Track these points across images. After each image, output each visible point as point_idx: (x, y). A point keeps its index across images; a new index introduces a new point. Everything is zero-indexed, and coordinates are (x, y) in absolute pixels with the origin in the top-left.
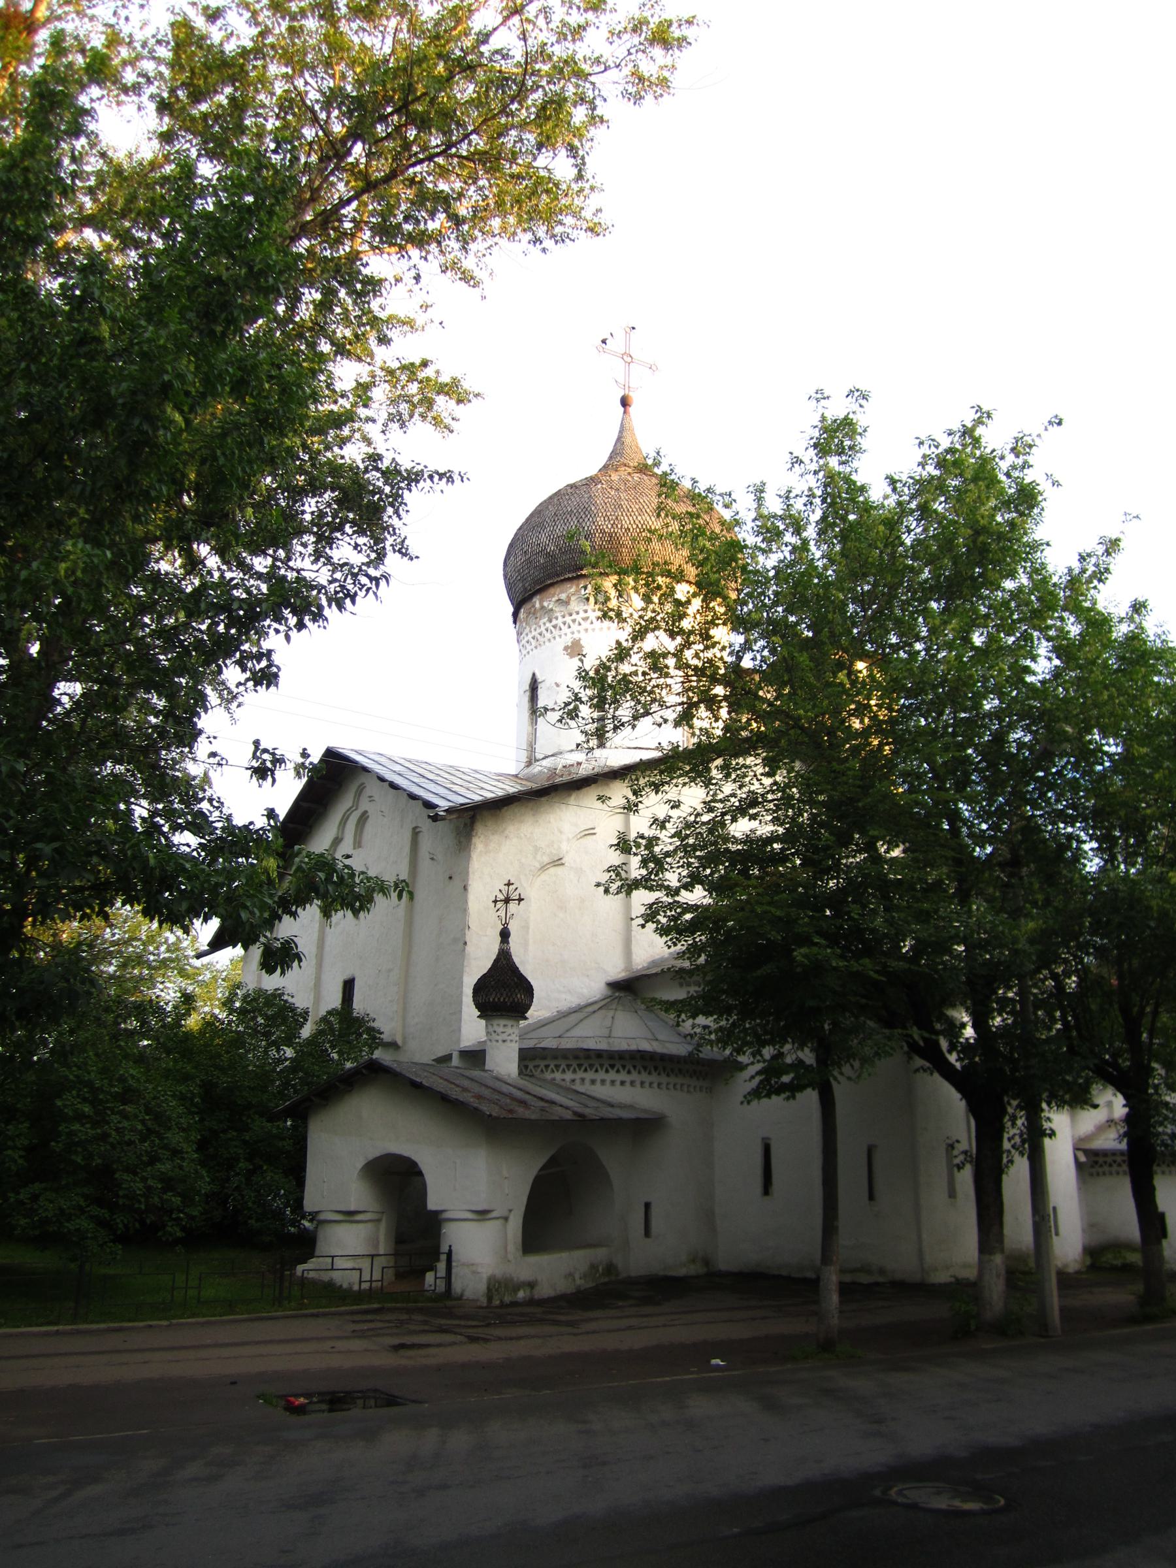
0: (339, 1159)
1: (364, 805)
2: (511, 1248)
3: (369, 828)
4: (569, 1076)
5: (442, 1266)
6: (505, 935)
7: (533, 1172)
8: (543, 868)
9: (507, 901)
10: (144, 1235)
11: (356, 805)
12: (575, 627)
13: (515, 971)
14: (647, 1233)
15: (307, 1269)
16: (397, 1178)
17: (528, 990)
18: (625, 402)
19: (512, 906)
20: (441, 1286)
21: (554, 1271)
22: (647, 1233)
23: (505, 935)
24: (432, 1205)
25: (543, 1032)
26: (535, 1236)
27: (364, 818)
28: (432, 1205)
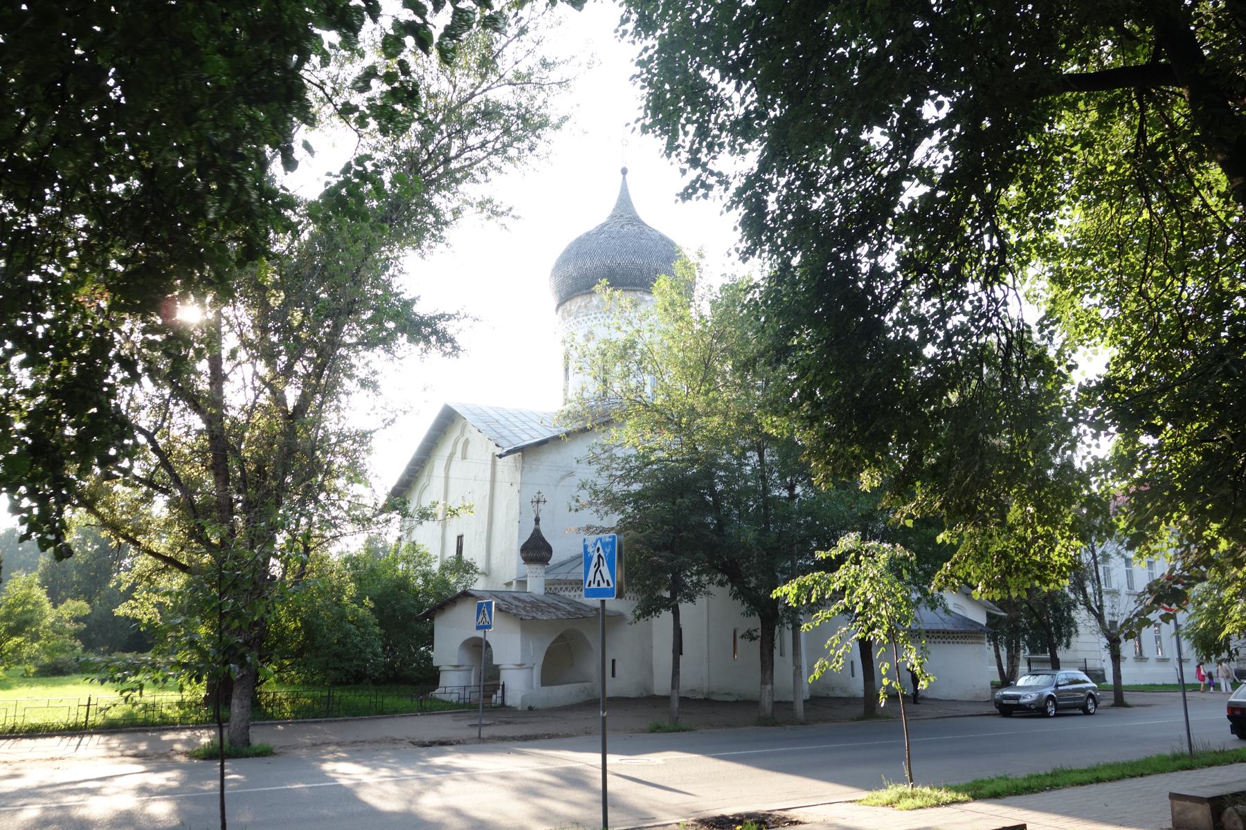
0: (449, 641)
1: (467, 435)
2: (535, 682)
3: (470, 449)
4: (572, 593)
5: (499, 692)
6: (537, 520)
7: (545, 649)
8: (563, 478)
9: (538, 502)
10: (357, 679)
11: (462, 433)
12: (589, 323)
13: (543, 539)
14: (613, 675)
15: (438, 693)
16: (478, 648)
17: (549, 550)
18: (624, 171)
19: (541, 505)
20: (499, 701)
21: (561, 693)
22: (613, 675)
23: (537, 520)
24: (495, 662)
25: (561, 570)
26: (546, 680)
27: (466, 443)
28: (495, 662)
